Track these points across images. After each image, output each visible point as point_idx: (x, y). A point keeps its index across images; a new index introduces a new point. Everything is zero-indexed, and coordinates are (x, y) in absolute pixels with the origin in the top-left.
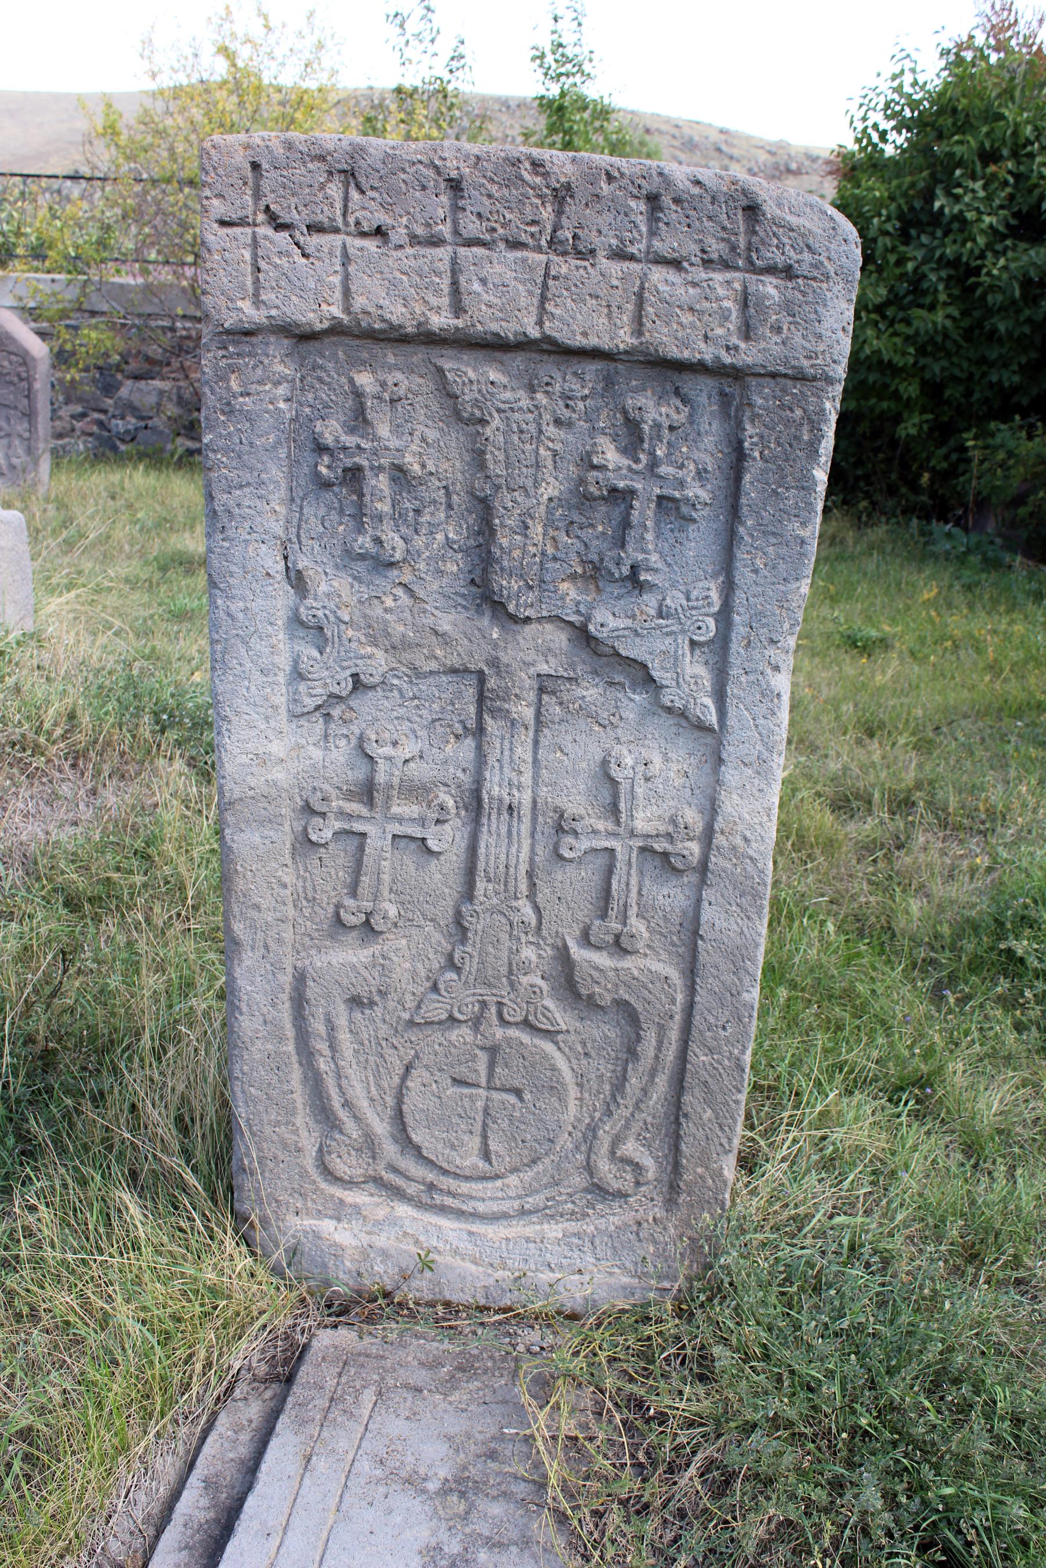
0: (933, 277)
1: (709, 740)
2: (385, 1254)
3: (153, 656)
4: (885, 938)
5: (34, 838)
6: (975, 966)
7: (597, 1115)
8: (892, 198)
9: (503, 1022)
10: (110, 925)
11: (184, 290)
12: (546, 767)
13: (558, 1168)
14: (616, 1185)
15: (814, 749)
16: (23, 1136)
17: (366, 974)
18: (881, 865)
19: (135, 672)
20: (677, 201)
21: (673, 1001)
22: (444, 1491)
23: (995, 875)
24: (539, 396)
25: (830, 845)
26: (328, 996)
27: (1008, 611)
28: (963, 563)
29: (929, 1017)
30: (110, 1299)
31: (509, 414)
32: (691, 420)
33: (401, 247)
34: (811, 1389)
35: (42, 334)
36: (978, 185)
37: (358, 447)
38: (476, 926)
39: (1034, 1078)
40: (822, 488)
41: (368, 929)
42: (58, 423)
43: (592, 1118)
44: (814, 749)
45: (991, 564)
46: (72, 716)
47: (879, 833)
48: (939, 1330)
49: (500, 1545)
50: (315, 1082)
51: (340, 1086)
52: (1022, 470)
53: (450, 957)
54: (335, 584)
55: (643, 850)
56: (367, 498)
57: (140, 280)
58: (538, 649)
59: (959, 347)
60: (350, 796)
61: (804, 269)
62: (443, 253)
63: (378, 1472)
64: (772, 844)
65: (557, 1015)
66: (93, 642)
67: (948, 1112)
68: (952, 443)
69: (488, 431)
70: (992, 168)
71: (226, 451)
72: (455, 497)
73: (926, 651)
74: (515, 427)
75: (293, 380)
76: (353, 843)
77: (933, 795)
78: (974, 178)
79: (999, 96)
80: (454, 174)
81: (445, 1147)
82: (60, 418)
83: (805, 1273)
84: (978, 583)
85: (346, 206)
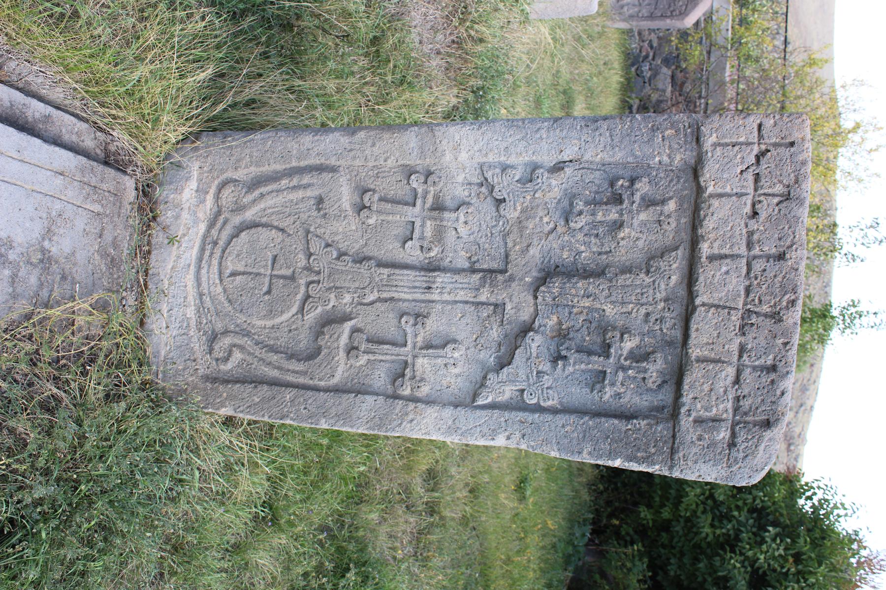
38: (363, 269)
41: (361, 208)
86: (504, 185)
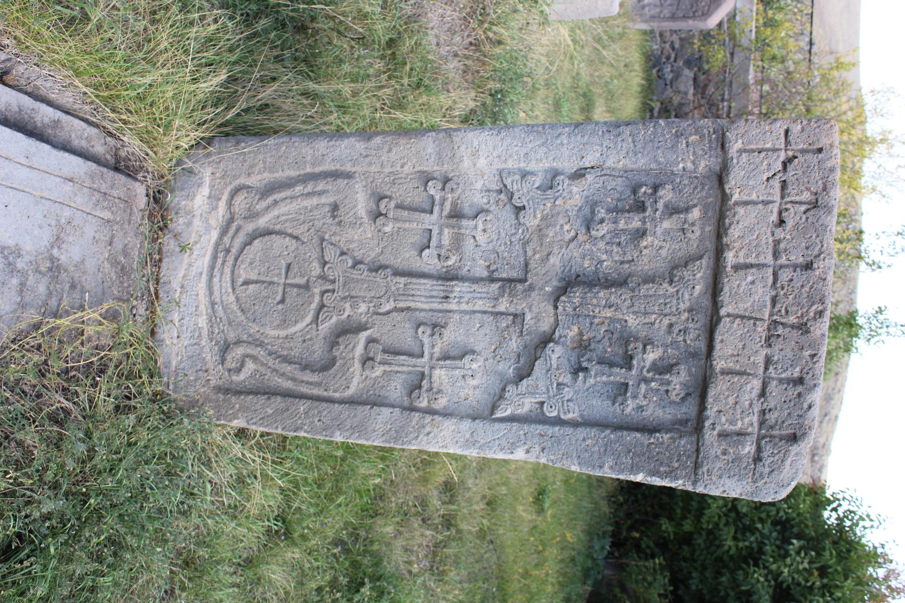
0: (752, 539)
1: (486, 413)
2: (189, 224)
3: (534, 89)
4: (371, 512)
5: (429, 21)
6: (355, 565)
7: (269, 347)
8: (798, 515)
9: (323, 293)
10: (379, 65)
11: (746, 107)
12: (470, 319)
13: (239, 324)
14: (229, 358)
15: (480, 470)
16: (257, 15)
17: (351, 214)
18: (413, 509)
19: (525, 79)
20: (799, 395)
21: (335, 391)
22: (52, 259)
23: (407, 576)
24: (686, 315)
25: (425, 480)
26: (338, 192)
27: (559, 583)
28: (587, 556)
29: (325, 538)
30: (163, 65)
31: (676, 297)
32: (672, 403)
33: (773, 235)
34: (111, 470)
35: (720, 25)
36: (806, 565)
37: (657, 210)
38: (379, 277)
39: (290, 599)
40: (632, 478)
41: (377, 215)
42: (669, 34)
43: (267, 344)
44: (480, 470)
45: (586, 573)
46: (500, 42)
47: (431, 508)
48: (145, 545)
49: (21, 291)
50: (289, 184)
51: (286, 198)
52: (642, 590)
53: (361, 262)
54: (577, 196)
55: (423, 374)
56: (627, 215)
57: (751, 82)
58: (539, 314)
59: (712, 554)
60: (454, 204)
61: (760, 468)
62: (769, 259)
63: (63, 221)
64: (425, 449)
65: (327, 324)
66: (542, 55)
67: (271, 548)
68: (656, 550)
69: (665, 285)
70: (816, 573)
71: (655, 133)
72: (627, 266)
73: (537, 535)
74: (668, 300)
75: (695, 172)
76: (427, 206)
77: (453, 540)
78: (810, 563)
79: (858, 577)
80: (815, 266)
81: (251, 259)
82: (671, 35)
83: (178, 467)
84: (575, 565)
85: (797, 203)
86: (524, 192)
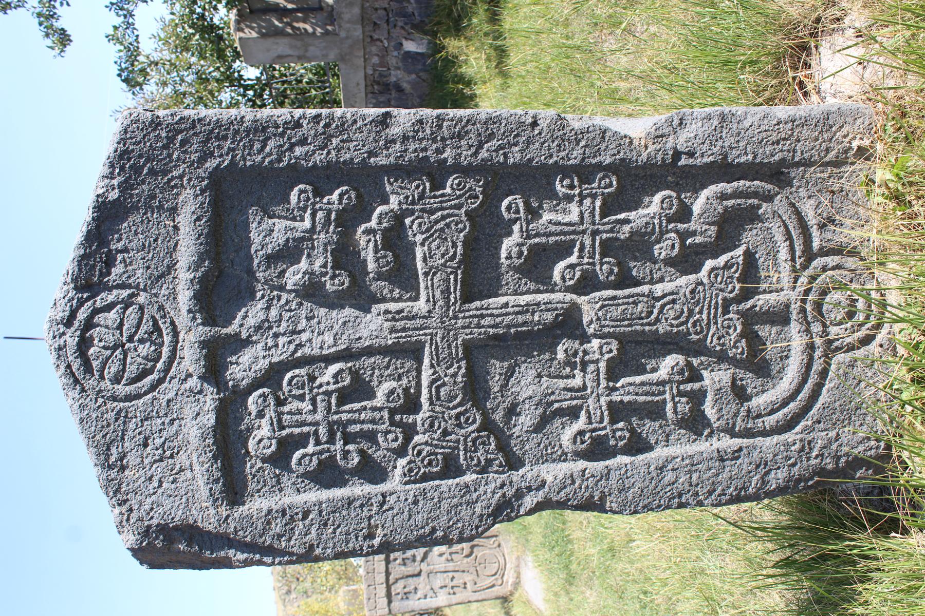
38: (462, 569)
41: (465, 584)
86: (431, 593)
